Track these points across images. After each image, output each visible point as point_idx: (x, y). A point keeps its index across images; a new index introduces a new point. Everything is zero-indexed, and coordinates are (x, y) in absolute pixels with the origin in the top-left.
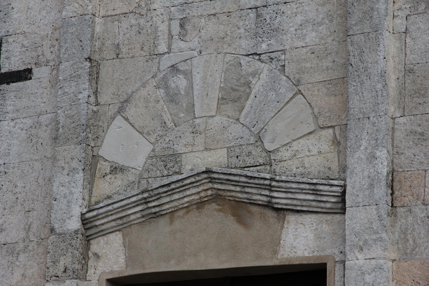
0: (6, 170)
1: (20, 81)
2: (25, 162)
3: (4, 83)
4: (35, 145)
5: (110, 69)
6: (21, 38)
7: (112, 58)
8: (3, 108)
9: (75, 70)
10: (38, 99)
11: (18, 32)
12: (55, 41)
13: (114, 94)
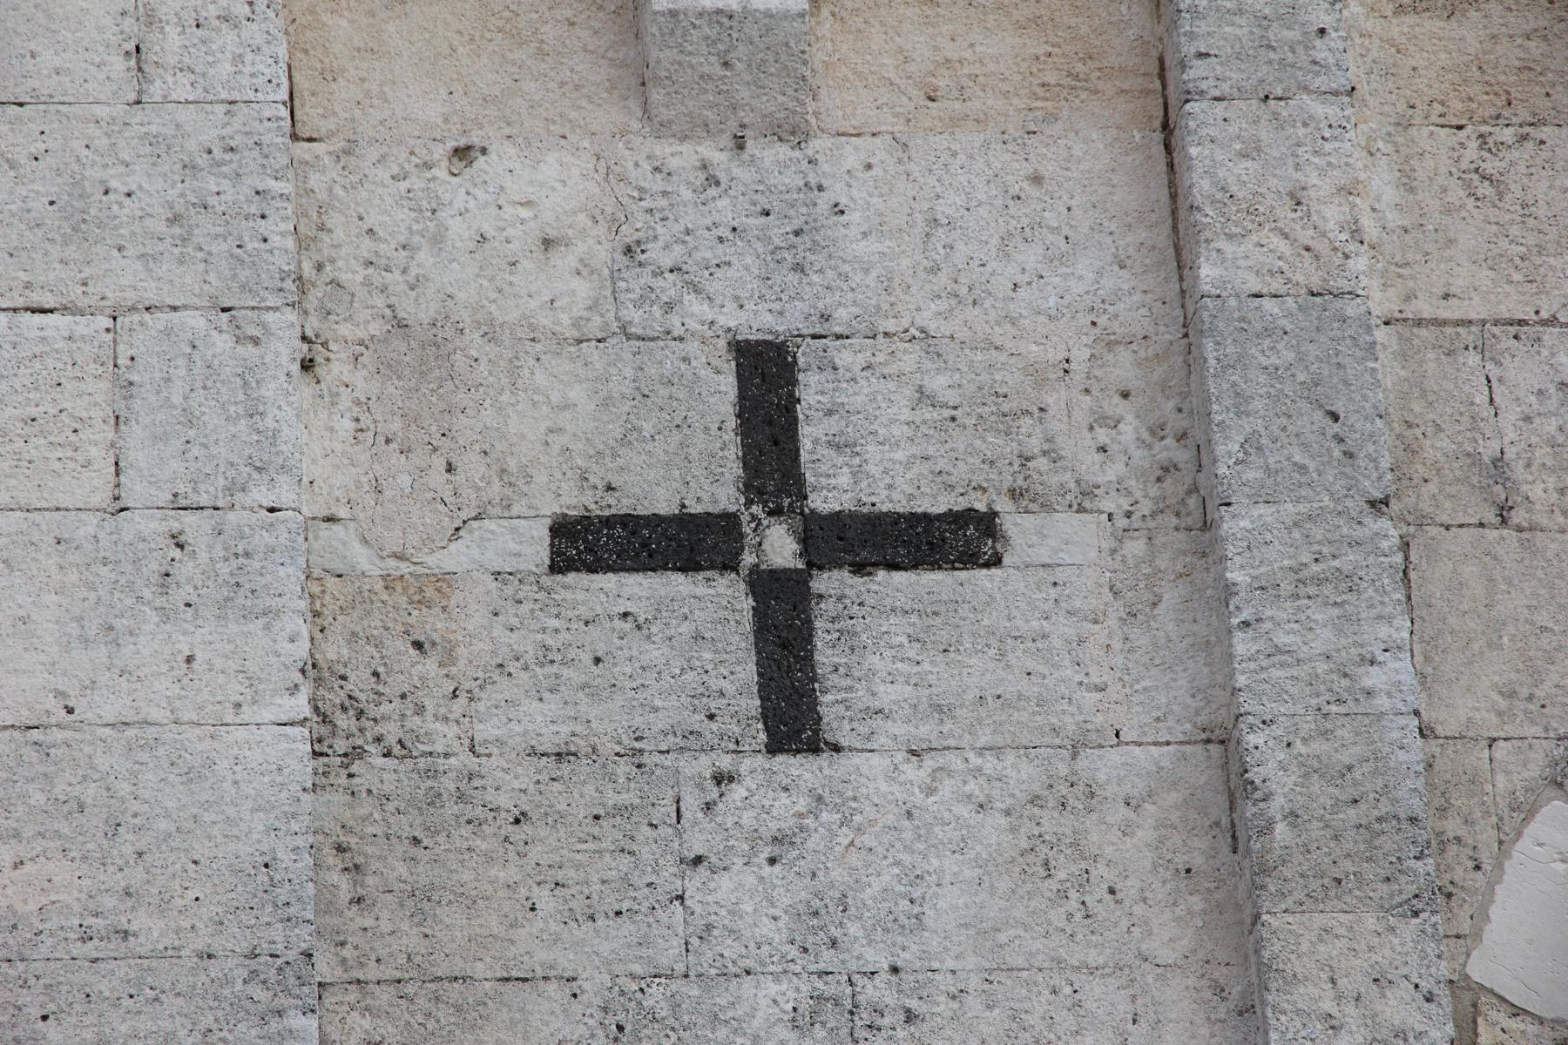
0: (913, 1003)
1: (935, 566)
2: (1025, 974)
3: (840, 567)
4: (1073, 894)
5: (1469, 570)
6: (909, 358)
7: (1474, 521)
8: (850, 689)
9: (1316, 547)
10: (1057, 667)
11: (890, 325)
12: (1117, 399)
13: (1512, 694)
